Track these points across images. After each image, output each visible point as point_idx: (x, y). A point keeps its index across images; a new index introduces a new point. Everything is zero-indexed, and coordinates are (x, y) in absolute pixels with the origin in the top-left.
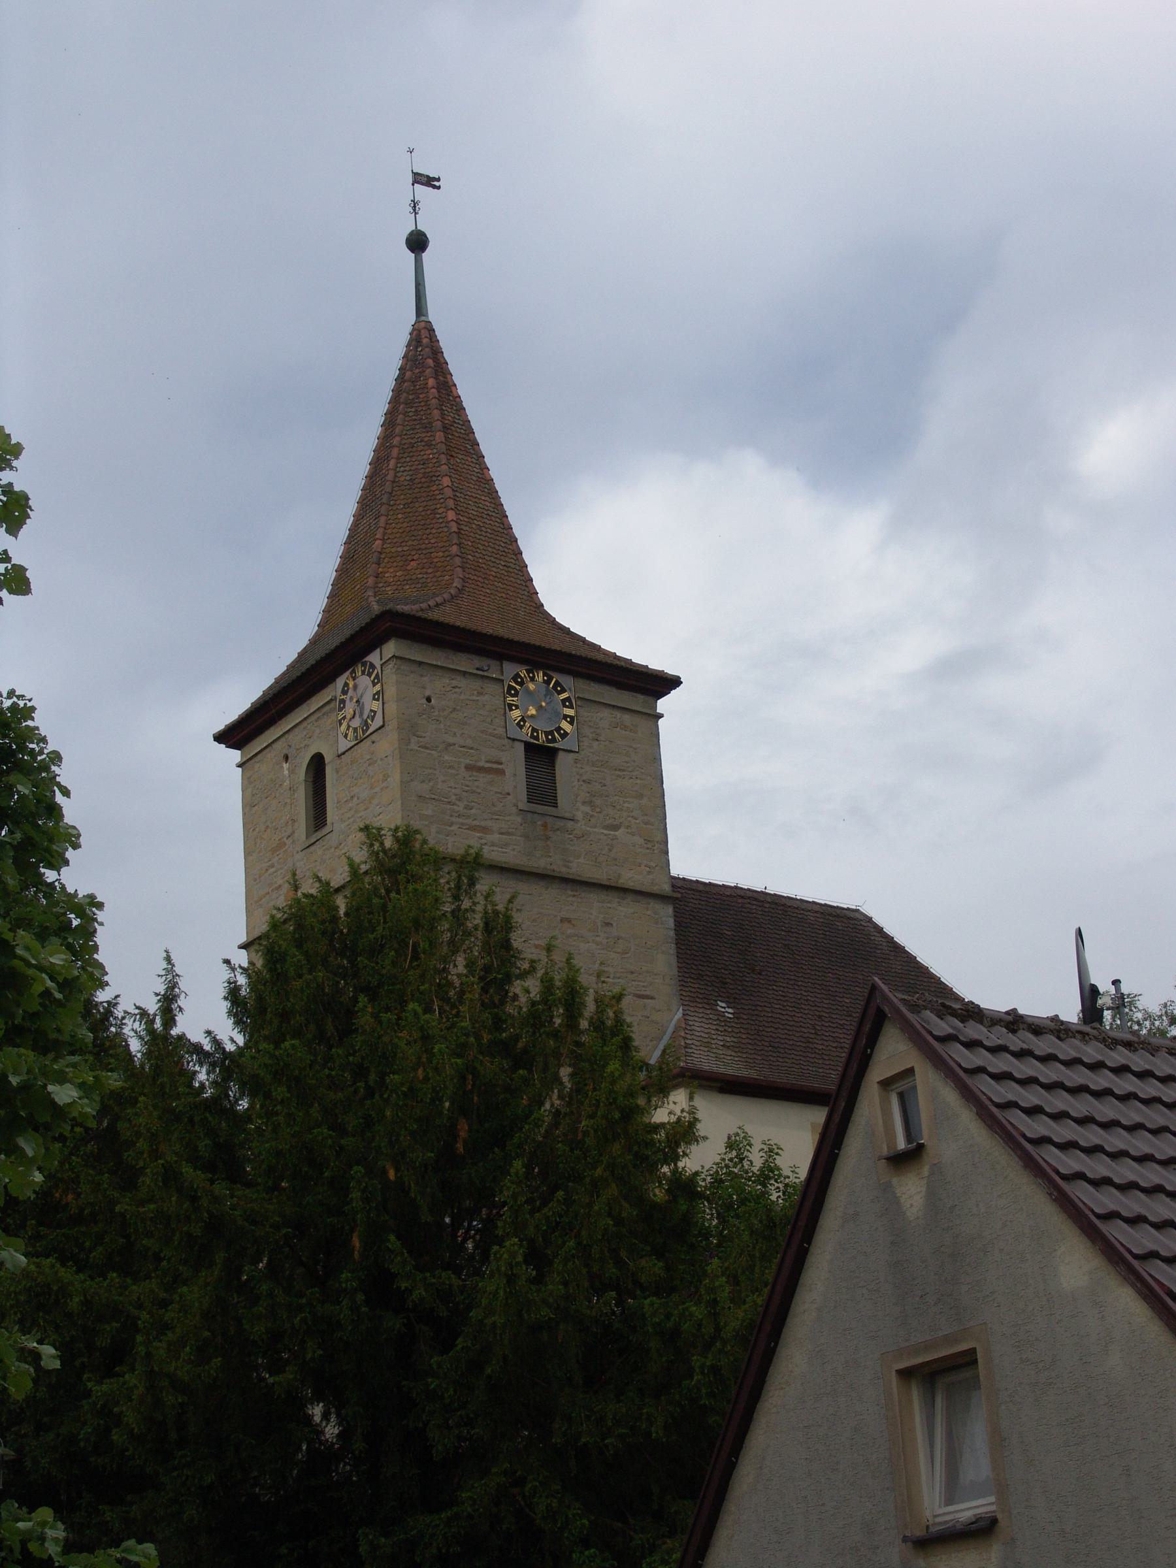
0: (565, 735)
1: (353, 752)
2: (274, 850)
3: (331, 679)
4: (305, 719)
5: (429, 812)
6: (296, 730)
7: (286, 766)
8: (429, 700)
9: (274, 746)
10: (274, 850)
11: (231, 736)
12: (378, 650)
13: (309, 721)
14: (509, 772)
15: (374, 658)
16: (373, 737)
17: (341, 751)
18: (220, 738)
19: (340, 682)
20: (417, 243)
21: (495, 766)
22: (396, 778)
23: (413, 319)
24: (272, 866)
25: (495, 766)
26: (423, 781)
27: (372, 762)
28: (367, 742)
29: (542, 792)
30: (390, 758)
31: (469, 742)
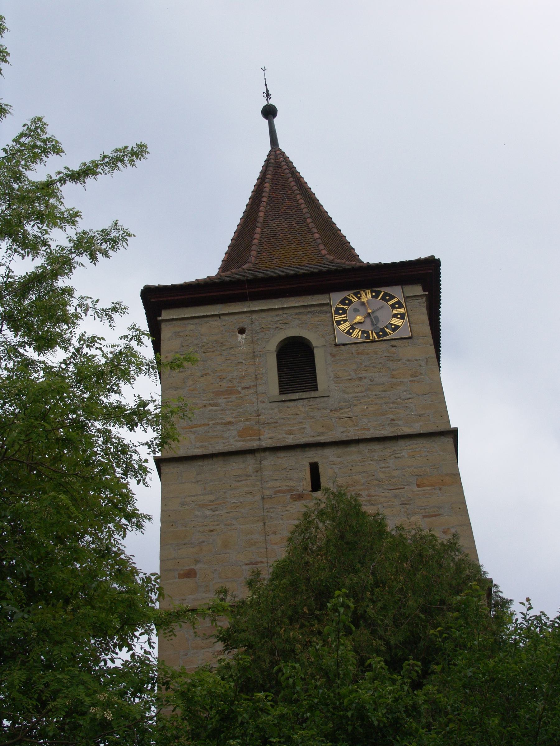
6: (264, 315)
20: (269, 112)
24: (216, 405)
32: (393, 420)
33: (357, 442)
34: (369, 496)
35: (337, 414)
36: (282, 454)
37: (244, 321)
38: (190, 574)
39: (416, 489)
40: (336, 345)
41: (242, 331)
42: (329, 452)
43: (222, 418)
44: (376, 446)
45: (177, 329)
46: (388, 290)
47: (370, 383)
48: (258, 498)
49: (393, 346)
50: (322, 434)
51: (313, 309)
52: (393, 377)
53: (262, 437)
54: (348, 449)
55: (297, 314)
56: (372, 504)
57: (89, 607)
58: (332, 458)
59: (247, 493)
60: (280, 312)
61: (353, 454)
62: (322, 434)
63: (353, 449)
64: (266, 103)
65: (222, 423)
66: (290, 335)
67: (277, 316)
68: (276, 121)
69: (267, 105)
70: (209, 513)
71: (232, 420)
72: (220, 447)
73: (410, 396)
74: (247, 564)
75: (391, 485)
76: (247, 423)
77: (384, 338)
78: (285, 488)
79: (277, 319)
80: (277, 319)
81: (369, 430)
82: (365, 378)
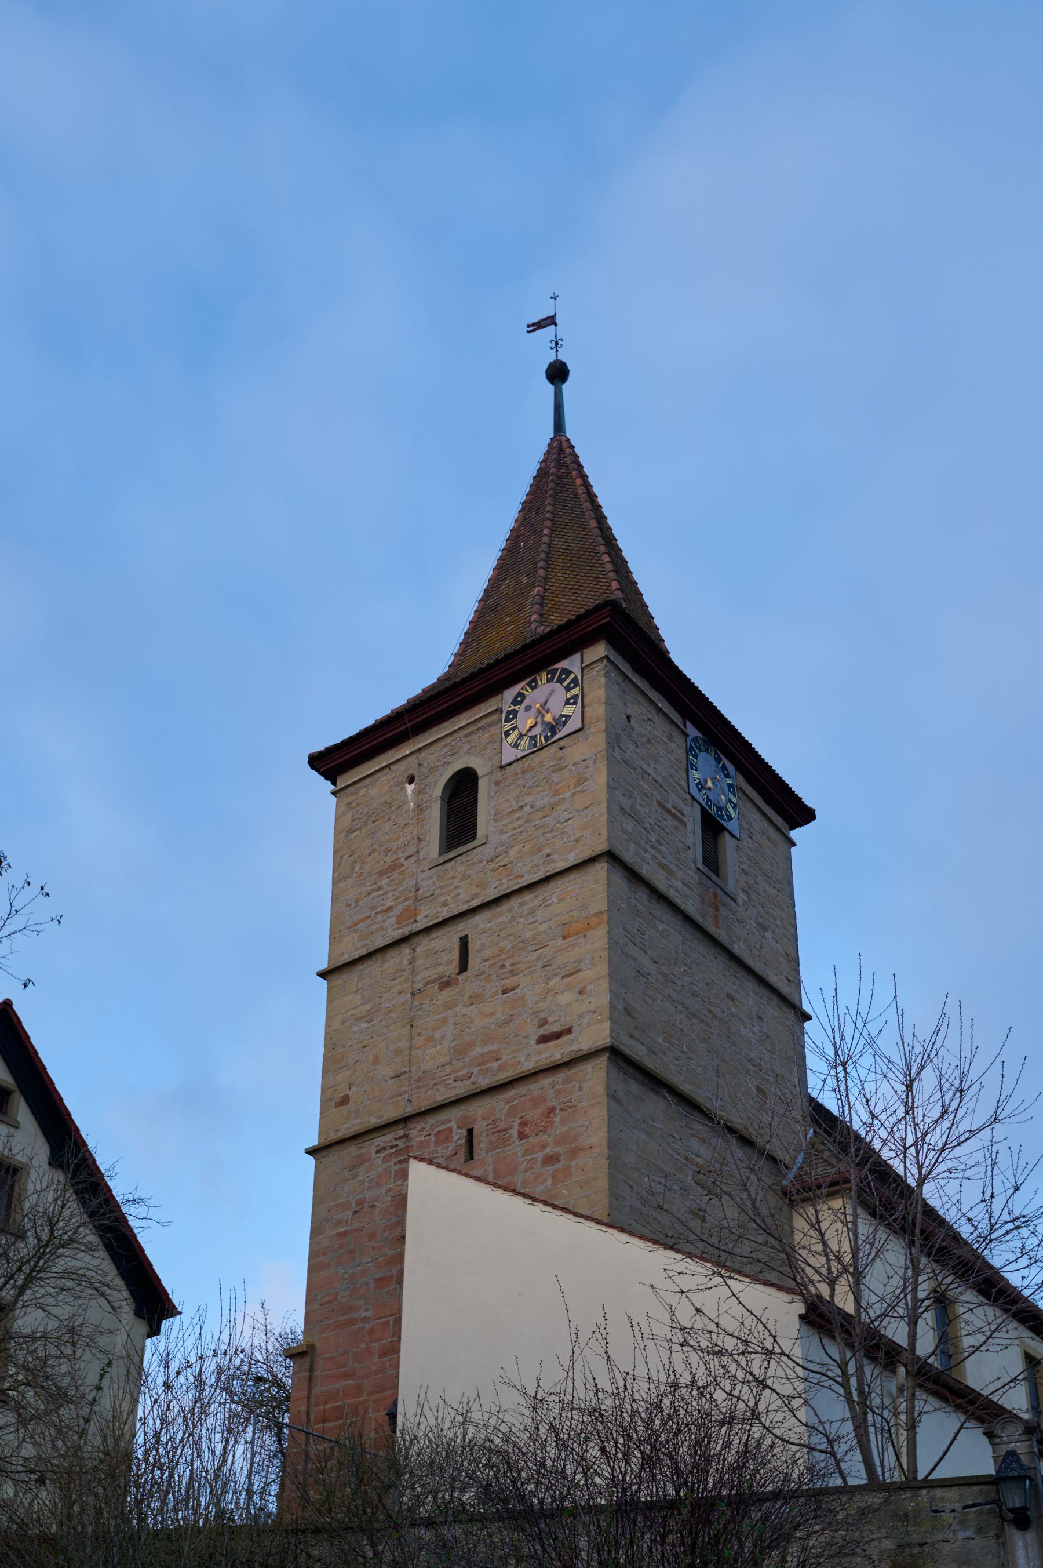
0: (730, 818)
1: (527, 762)
2: (382, 874)
3: (496, 689)
4: (450, 734)
5: (629, 828)
6: (432, 749)
7: (410, 788)
8: (629, 718)
9: (394, 768)
10: (382, 874)
11: (331, 763)
12: (578, 656)
13: (455, 736)
14: (689, 826)
15: (572, 663)
16: (562, 743)
17: (504, 763)
18: (317, 761)
19: (509, 694)
20: (558, 373)
21: (679, 815)
22: (600, 779)
23: (551, 434)
24: (380, 888)
25: (679, 815)
26: (624, 795)
27: (557, 769)
28: (552, 749)
29: (712, 861)
30: (590, 763)
31: (660, 779)
32: (549, 855)
33: (507, 896)
34: (512, 965)
35: (493, 865)
36: (434, 934)
37: (409, 766)
38: (344, 1101)
39: (560, 941)
40: (502, 767)
41: (411, 780)
42: (480, 920)
43: (383, 905)
44: (527, 897)
45: (349, 800)
46: (563, 664)
47: (531, 810)
48: (409, 996)
49: (561, 749)
50: (476, 896)
51: (483, 722)
52: (556, 793)
53: (418, 919)
54: (499, 909)
55: (466, 736)
56: (514, 975)
57: (924, 1492)
58: (482, 926)
59: (400, 993)
60: (448, 740)
61: (504, 913)
62: (476, 896)
63: (504, 907)
64: (553, 358)
65: (382, 911)
66: (456, 770)
67: (445, 746)
68: (566, 387)
69: (555, 362)
70: (364, 1025)
71: (392, 903)
72: (380, 942)
73: (571, 816)
74: (392, 1078)
75: (536, 944)
76: (406, 903)
77: (556, 738)
78: (434, 977)
79: (445, 750)
80: (445, 750)
81: (522, 876)
82: (526, 805)
